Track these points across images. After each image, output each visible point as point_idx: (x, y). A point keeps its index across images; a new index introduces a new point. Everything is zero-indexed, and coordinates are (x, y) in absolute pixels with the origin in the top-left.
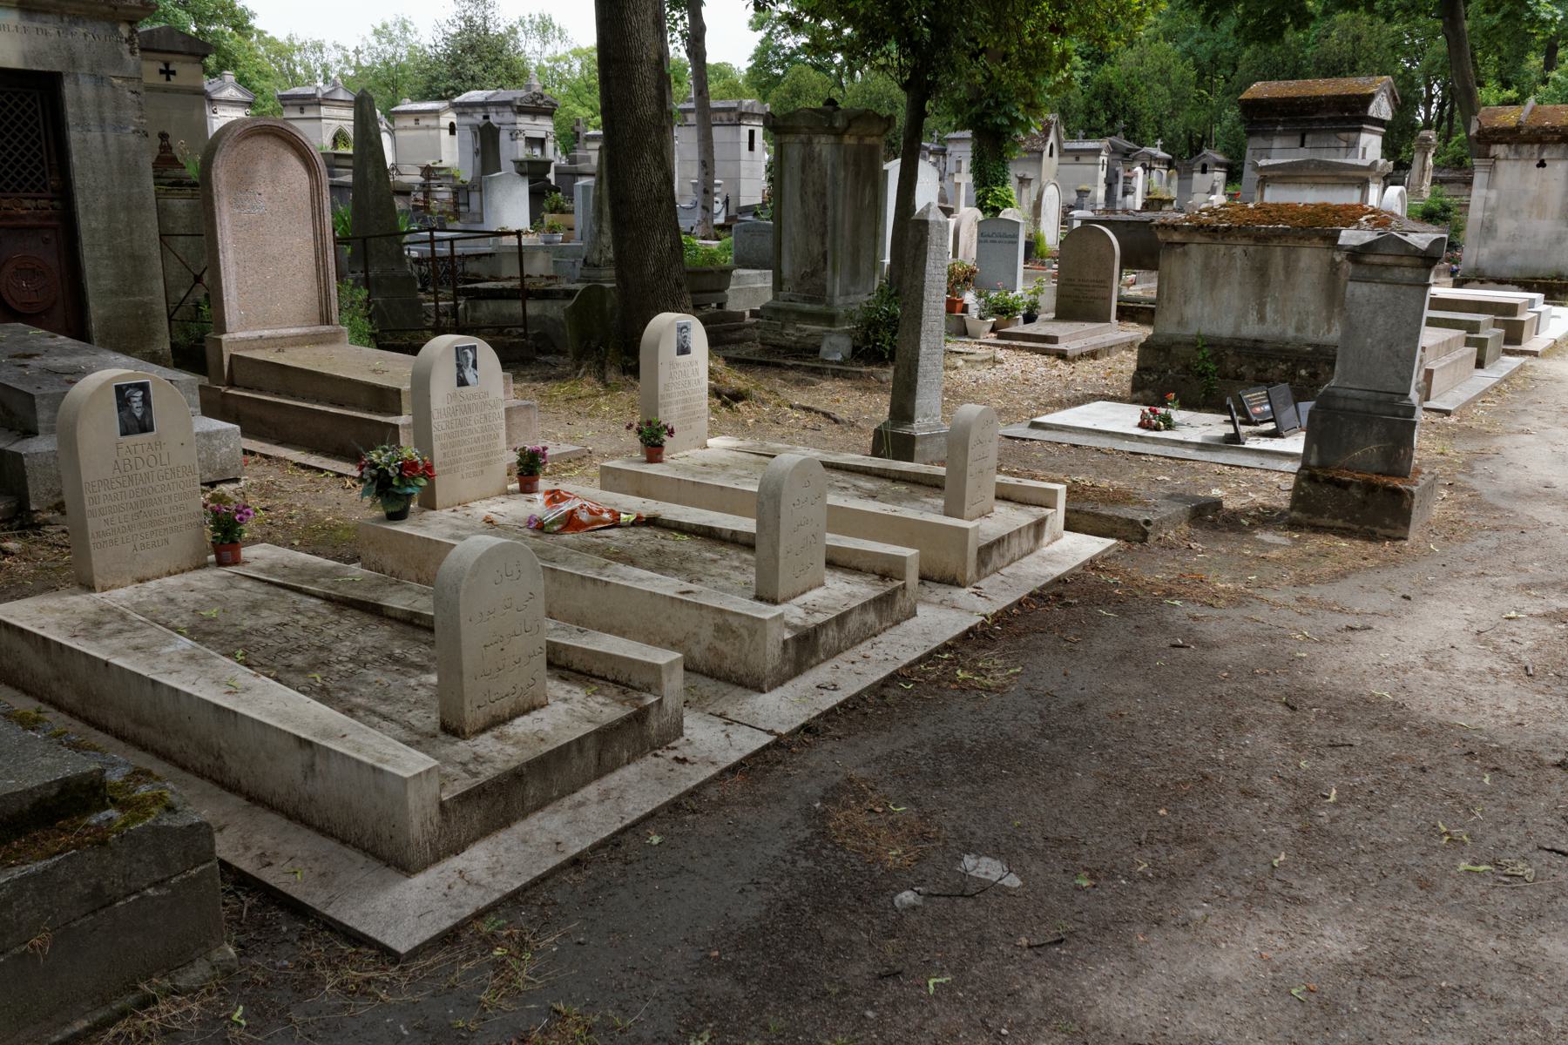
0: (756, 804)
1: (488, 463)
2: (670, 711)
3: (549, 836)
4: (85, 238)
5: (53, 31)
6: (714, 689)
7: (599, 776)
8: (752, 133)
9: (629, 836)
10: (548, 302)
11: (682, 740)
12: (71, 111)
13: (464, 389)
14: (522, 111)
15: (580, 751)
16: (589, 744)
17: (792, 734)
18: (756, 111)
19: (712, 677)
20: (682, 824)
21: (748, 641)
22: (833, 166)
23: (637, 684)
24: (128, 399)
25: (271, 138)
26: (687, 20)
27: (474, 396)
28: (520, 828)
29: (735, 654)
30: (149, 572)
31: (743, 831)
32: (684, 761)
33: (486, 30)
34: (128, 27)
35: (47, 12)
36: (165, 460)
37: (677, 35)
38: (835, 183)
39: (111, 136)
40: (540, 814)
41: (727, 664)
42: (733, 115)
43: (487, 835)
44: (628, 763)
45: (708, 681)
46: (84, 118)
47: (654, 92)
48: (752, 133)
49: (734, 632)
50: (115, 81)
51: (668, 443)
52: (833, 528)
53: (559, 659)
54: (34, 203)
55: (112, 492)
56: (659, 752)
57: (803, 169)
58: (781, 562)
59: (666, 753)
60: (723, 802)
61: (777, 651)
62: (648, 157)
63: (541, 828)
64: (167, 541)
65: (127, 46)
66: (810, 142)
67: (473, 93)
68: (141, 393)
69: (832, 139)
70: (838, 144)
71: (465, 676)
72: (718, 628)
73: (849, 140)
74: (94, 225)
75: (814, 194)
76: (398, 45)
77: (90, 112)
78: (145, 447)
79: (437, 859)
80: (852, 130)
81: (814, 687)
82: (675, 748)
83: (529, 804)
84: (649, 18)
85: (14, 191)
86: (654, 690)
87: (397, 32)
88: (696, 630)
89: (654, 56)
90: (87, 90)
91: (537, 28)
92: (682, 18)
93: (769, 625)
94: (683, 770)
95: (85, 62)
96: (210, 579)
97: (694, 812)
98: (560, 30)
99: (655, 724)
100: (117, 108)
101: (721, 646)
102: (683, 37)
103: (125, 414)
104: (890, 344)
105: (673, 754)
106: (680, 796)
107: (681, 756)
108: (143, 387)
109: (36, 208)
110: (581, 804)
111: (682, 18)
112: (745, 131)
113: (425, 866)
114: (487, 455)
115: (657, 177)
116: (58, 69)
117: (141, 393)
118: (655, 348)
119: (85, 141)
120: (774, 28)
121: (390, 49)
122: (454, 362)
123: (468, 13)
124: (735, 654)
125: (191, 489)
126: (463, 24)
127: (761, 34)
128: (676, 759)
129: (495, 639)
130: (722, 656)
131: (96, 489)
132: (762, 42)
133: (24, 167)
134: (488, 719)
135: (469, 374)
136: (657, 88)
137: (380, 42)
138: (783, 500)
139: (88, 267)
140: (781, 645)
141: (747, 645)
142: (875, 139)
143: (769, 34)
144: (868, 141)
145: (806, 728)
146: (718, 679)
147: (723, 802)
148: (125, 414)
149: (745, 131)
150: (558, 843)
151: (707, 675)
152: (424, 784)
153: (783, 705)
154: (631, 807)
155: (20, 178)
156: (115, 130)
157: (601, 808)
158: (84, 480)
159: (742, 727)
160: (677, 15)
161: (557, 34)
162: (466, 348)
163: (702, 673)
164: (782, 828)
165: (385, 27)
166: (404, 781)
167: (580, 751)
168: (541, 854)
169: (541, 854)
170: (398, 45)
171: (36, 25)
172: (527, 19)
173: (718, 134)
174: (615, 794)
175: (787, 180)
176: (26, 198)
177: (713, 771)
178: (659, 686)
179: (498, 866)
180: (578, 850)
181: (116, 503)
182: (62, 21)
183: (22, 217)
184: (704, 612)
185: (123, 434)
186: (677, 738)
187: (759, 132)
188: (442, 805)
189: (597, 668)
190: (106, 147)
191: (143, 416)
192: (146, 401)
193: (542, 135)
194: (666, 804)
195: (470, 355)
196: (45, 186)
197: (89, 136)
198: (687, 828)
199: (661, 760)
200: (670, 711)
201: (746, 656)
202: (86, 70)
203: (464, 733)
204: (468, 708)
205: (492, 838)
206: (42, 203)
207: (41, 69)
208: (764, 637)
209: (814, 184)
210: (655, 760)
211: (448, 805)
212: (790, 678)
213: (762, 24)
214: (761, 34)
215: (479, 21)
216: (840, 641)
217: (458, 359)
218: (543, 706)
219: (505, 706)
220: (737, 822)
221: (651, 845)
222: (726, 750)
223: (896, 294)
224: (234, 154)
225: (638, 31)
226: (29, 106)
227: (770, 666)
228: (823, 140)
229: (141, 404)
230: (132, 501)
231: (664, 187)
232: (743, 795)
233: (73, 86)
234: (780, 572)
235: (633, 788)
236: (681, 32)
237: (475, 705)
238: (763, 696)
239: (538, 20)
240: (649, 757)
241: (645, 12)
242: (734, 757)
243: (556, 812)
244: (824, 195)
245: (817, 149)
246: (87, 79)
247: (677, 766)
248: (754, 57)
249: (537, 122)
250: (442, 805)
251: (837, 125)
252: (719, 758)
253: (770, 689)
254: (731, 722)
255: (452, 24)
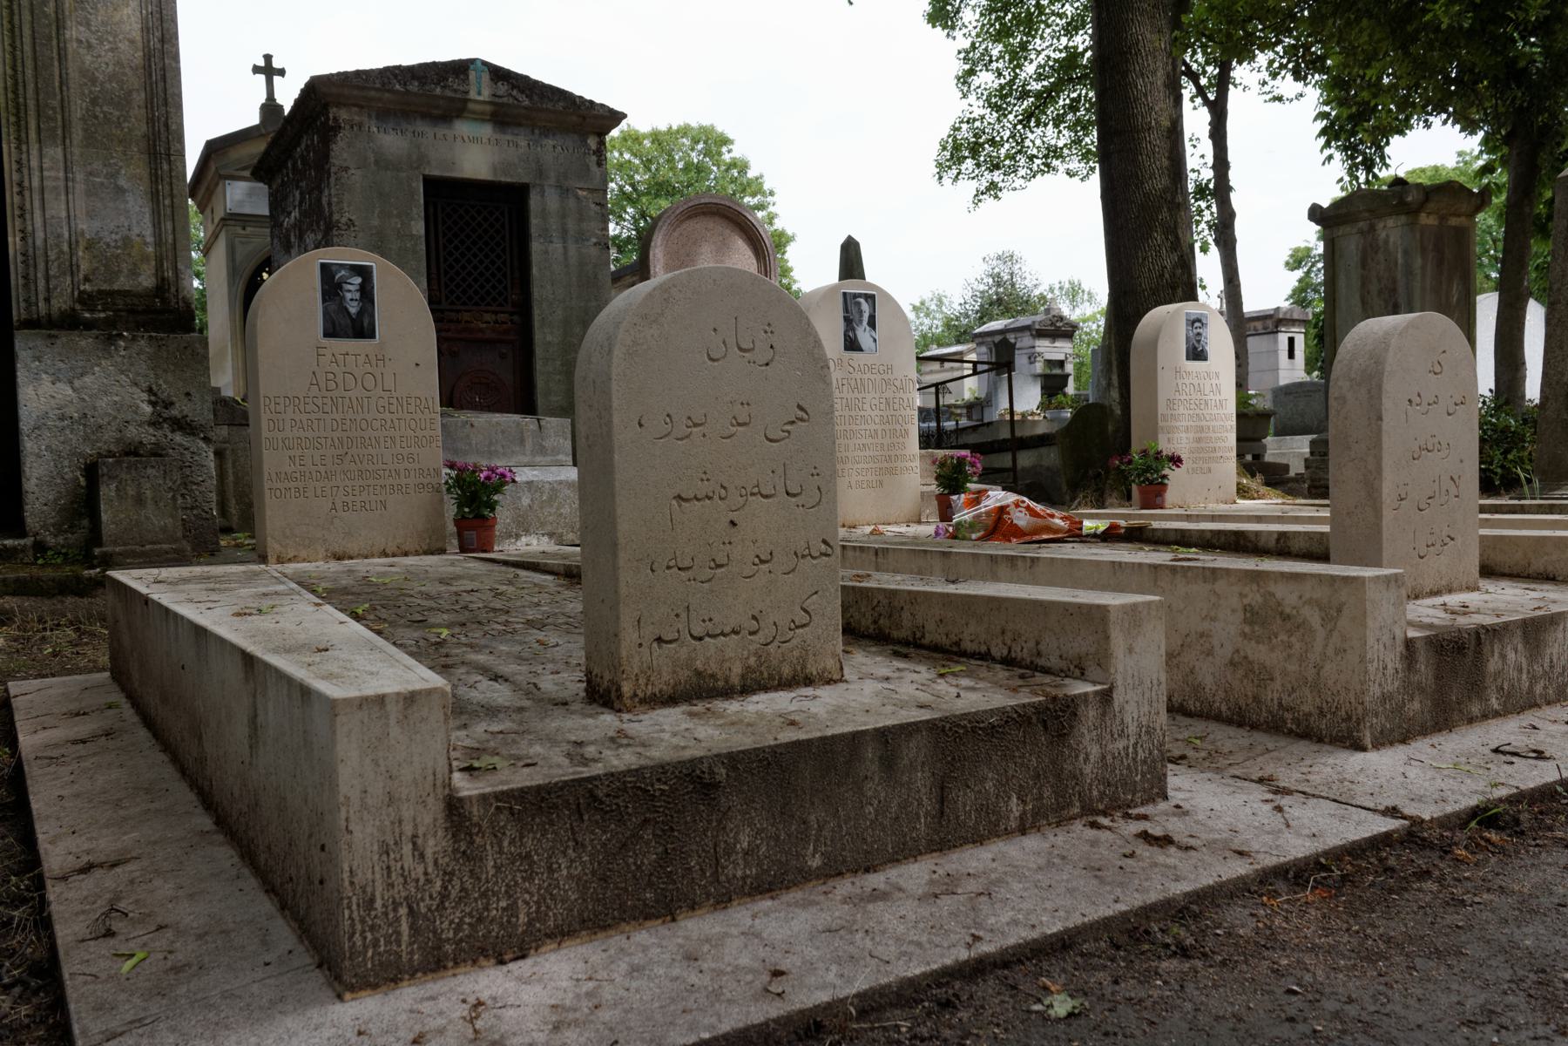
0: (1371, 958)
1: (892, 471)
2: (1132, 729)
3: (762, 953)
4: (539, 351)
5: (523, 143)
6: (1245, 742)
7: (941, 844)
8: (1291, 341)
9: (987, 988)
10: (1043, 450)
11: (1162, 806)
12: (535, 222)
13: (855, 355)
14: (1041, 334)
15: (889, 763)
16: (913, 750)
17: (1445, 822)
18: (1296, 316)
19: (1240, 725)
20: (1146, 978)
21: (1321, 634)
22: (1406, 252)
23: (1054, 662)
24: (339, 286)
25: (717, 218)
26: (1214, 209)
27: (870, 368)
28: (697, 926)
29: (1292, 667)
30: (352, 547)
31: (1337, 1015)
32: (1165, 841)
33: (1013, 285)
34: (597, 139)
35: (520, 125)
36: (389, 384)
37: (1203, 225)
38: (1409, 272)
39: (572, 249)
40: (767, 904)
41: (1273, 694)
42: (1270, 323)
43: (605, 928)
44: (1023, 831)
45: (1231, 731)
46: (547, 230)
47: (1166, 163)
48: (1291, 341)
49: (1286, 618)
50: (580, 192)
51: (1175, 477)
52: (1481, 512)
53: (899, 627)
54: (494, 317)
55: (304, 417)
56: (1105, 821)
57: (1364, 264)
58: (1388, 515)
59: (1121, 823)
60: (1270, 940)
61: (1393, 660)
62: (1158, 236)
63: (751, 934)
64: (384, 505)
65: (594, 158)
66: (1372, 228)
67: (993, 323)
68: (358, 280)
69: (1403, 219)
70: (1412, 225)
71: (623, 557)
72: (1252, 616)
73: (1426, 220)
74: (549, 338)
75: (1380, 292)
76: (934, 318)
77: (554, 223)
78: (361, 359)
79: (436, 962)
80: (1431, 206)
81: (1486, 751)
82: (1145, 817)
83: (737, 870)
84: (1160, 79)
85: (476, 304)
86: (1092, 671)
87: (933, 307)
88: (1206, 625)
89: (1166, 123)
90: (552, 200)
91: (1067, 294)
92: (1208, 207)
93: (1372, 593)
94: (1161, 859)
95: (552, 174)
96: (451, 563)
97: (1184, 952)
98: (1089, 293)
99: (1095, 751)
100: (581, 219)
101: (1258, 653)
102: (1210, 228)
103: (333, 306)
104: (1502, 467)
105: (1135, 827)
106: (1147, 911)
107: (1157, 831)
108: (364, 272)
109: (496, 322)
110: (877, 896)
111: (1208, 207)
112: (1283, 339)
113: (388, 975)
114: (889, 459)
115: (1169, 260)
116: (525, 180)
117: (358, 280)
118: (1152, 345)
119: (546, 252)
120: (1313, 266)
121: (927, 321)
122: (840, 314)
123: (996, 270)
124: (1292, 667)
125: (427, 433)
126: (991, 281)
127: (1299, 273)
128: (1145, 836)
129: (704, 488)
130: (1260, 675)
131: (281, 408)
132: (1300, 281)
133: (488, 281)
134: (684, 674)
135: (864, 335)
136: (1169, 158)
137: (918, 318)
138: (1389, 386)
139: (540, 382)
140: (1400, 648)
141: (1318, 645)
142: (1463, 219)
143: (1308, 273)
144: (1454, 221)
145: (1484, 817)
146: (1254, 727)
147: (1270, 940)
148: (333, 306)
149: (1283, 339)
150: (777, 973)
151: (1229, 722)
152: (395, 731)
153: (1413, 773)
154: (1006, 916)
155: (463, 261)
156: (577, 242)
157: (925, 911)
158: (262, 393)
159: (1313, 801)
160: (1203, 204)
161: (1086, 297)
162: (860, 295)
163: (1218, 718)
164: (1470, 1023)
165: (923, 303)
166: (332, 705)
167: (889, 763)
168: (716, 995)
169: (716, 995)
170: (934, 318)
171: (509, 137)
172: (1057, 286)
173: (1252, 343)
174: (973, 886)
175: (1342, 282)
176: (487, 312)
177: (1239, 868)
178: (1103, 659)
179: (585, 1005)
180: (823, 997)
181: (310, 434)
182: (533, 133)
183: (481, 330)
184: (1220, 585)
185: (326, 335)
186: (1151, 800)
187: (1300, 341)
188: (454, 806)
189: (971, 634)
190: (566, 259)
191: (360, 313)
192: (366, 292)
193: (1061, 357)
194: (1106, 924)
195: (865, 307)
196: (506, 300)
197: (551, 247)
198: (1157, 990)
199: (1104, 835)
200: (1132, 729)
201: (1318, 668)
202: (552, 181)
203: (620, 696)
204: (629, 637)
205: (616, 940)
206: (502, 317)
207: (509, 180)
208: (1361, 619)
209: (1379, 281)
210: (1091, 833)
211: (476, 811)
212: (1424, 732)
213: (1300, 262)
214: (1299, 273)
215: (1006, 277)
216: (1533, 679)
217: (846, 310)
218: (829, 682)
219: (731, 657)
220: (1317, 994)
221: (1044, 1017)
222: (1276, 833)
223: (1507, 402)
224: (676, 234)
225: (1146, 95)
226: (497, 220)
227: (1375, 690)
228: (1390, 222)
229: (357, 295)
230: (336, 435)
231: (1179, 271)
232: (1327, 931)
233: (539, 198)
234: (1385, 534)
235: (1021, 878)
236: (1207, 222)
237: (649, 632)
238: (1359, 757)
239: (1067, 286)
240: (1078, 826)
241: (1154, 73)
242: (1297, 848)
243: (807, 904)
244: (1394, 290)
245: (1383, 235)
246: (553, 190)
247: (1143, 850)
248: (1291, 297)
249: (1057, 344)
250: (454, 806)
251: (1410, 199)
252: (1255, 846)
253: (1378, 745)
254: (1286, 792)
255: (980, 281)
